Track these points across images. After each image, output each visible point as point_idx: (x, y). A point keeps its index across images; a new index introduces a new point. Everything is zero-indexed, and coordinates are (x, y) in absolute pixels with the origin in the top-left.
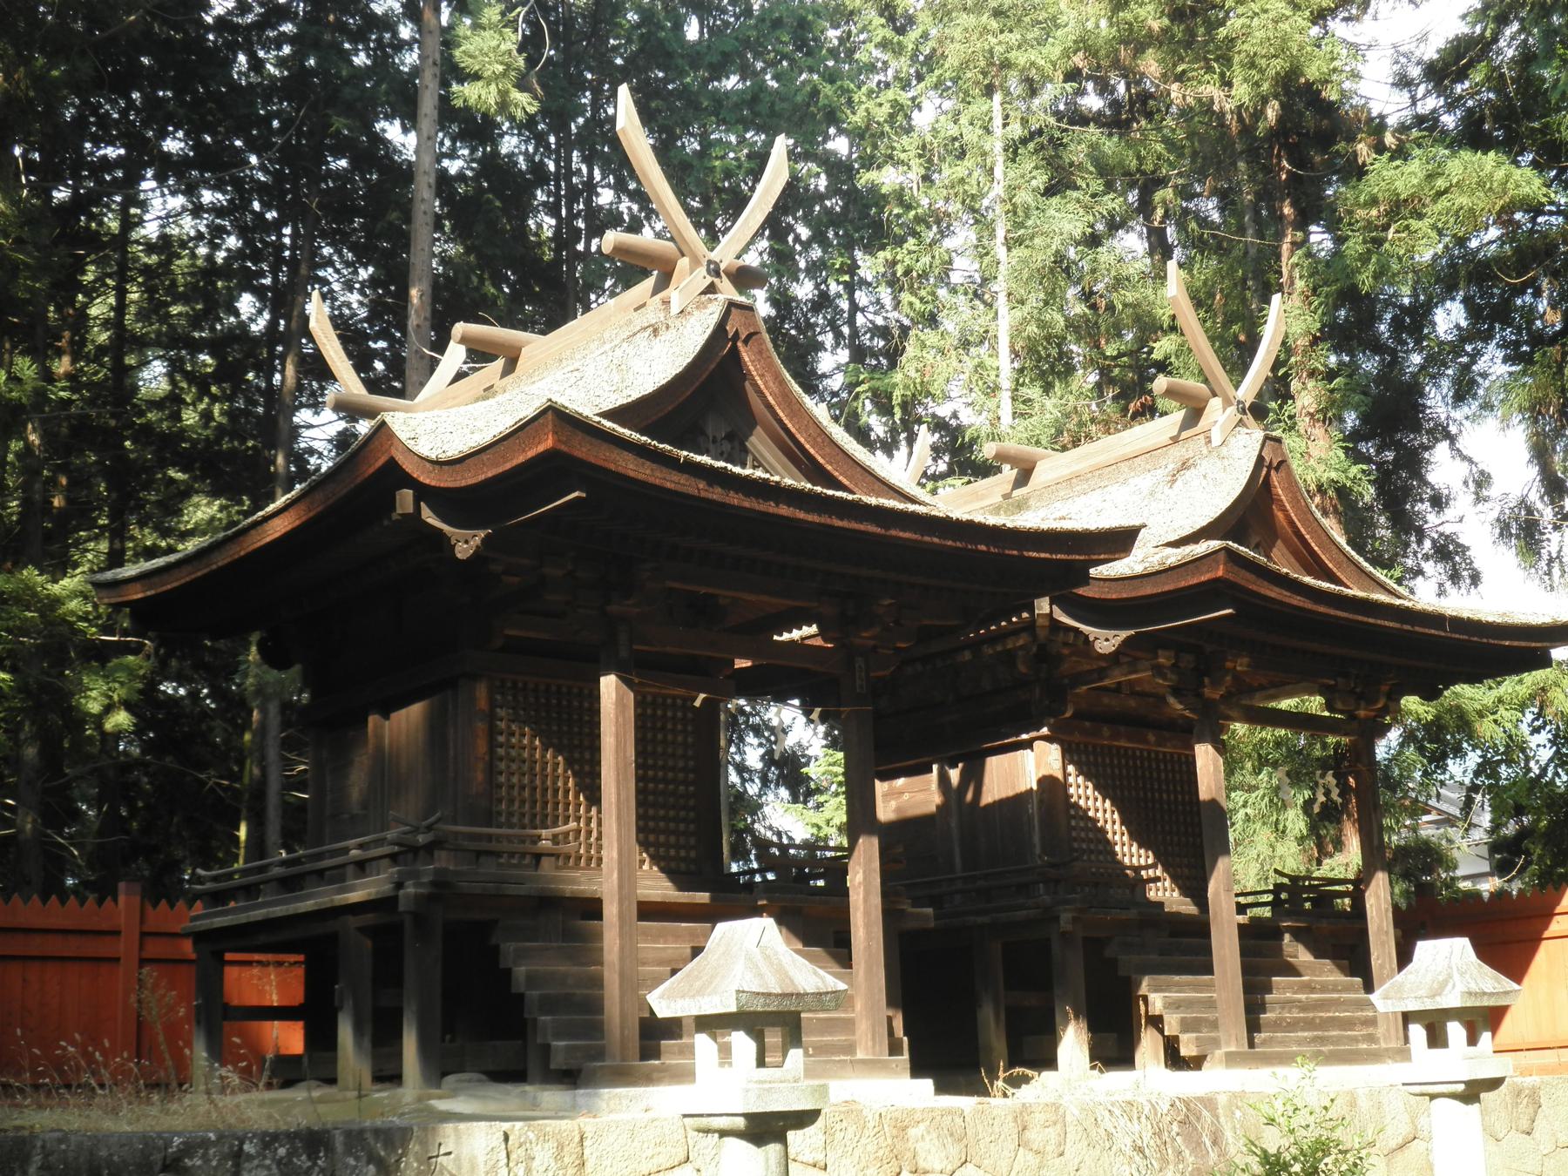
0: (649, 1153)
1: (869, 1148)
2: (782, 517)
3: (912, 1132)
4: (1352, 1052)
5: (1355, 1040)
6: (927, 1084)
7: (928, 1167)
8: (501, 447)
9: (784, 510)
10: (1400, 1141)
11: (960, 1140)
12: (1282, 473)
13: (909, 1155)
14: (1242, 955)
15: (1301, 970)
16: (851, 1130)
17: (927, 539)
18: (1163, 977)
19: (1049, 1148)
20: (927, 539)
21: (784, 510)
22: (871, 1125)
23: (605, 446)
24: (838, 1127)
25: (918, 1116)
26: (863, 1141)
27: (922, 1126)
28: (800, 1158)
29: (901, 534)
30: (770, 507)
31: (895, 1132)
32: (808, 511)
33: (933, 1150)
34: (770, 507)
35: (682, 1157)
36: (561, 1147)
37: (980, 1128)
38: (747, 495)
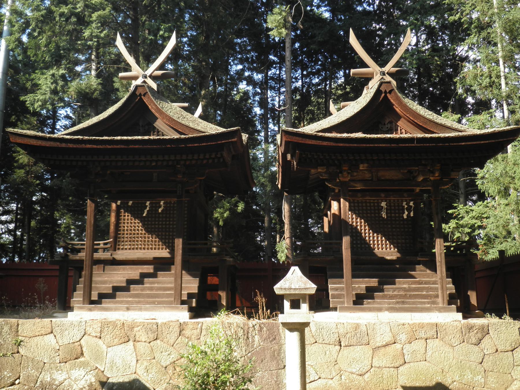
0: (39, 330)
1: (117, 333)
2: (88, 148)
3: (135, 329)
4: (413, 308)
5: (424, 303)
6: (460, 315)
7: (139, 340)
8: (432, 123)
9: (89, 146)
10: (384, 343)
11: (154, 332)
12: (393, 94)
13: (133, 336)
14: (352, 271)
15: (417, 277)
16: (111, 328)
17: (145, 147)
18: (310, 282)
19: (193, 337)
20: (145, 147)
21: (89, 146)
22: (119, 326)
23: (25, 139)
24: (106, 326)
25: (138, 324)
26: (115, 331)
27: (139, 327)
28: (91, 334)
29: (135, 147)
30: (83, 146)
31: (128, 329)
32: (97, 145)
33: (143, 335)
34: (83, 146)
35: (50, 331)
36: (11, 327)
37: (164, 329)
38: (74, 144)
